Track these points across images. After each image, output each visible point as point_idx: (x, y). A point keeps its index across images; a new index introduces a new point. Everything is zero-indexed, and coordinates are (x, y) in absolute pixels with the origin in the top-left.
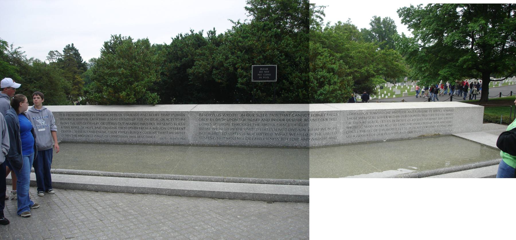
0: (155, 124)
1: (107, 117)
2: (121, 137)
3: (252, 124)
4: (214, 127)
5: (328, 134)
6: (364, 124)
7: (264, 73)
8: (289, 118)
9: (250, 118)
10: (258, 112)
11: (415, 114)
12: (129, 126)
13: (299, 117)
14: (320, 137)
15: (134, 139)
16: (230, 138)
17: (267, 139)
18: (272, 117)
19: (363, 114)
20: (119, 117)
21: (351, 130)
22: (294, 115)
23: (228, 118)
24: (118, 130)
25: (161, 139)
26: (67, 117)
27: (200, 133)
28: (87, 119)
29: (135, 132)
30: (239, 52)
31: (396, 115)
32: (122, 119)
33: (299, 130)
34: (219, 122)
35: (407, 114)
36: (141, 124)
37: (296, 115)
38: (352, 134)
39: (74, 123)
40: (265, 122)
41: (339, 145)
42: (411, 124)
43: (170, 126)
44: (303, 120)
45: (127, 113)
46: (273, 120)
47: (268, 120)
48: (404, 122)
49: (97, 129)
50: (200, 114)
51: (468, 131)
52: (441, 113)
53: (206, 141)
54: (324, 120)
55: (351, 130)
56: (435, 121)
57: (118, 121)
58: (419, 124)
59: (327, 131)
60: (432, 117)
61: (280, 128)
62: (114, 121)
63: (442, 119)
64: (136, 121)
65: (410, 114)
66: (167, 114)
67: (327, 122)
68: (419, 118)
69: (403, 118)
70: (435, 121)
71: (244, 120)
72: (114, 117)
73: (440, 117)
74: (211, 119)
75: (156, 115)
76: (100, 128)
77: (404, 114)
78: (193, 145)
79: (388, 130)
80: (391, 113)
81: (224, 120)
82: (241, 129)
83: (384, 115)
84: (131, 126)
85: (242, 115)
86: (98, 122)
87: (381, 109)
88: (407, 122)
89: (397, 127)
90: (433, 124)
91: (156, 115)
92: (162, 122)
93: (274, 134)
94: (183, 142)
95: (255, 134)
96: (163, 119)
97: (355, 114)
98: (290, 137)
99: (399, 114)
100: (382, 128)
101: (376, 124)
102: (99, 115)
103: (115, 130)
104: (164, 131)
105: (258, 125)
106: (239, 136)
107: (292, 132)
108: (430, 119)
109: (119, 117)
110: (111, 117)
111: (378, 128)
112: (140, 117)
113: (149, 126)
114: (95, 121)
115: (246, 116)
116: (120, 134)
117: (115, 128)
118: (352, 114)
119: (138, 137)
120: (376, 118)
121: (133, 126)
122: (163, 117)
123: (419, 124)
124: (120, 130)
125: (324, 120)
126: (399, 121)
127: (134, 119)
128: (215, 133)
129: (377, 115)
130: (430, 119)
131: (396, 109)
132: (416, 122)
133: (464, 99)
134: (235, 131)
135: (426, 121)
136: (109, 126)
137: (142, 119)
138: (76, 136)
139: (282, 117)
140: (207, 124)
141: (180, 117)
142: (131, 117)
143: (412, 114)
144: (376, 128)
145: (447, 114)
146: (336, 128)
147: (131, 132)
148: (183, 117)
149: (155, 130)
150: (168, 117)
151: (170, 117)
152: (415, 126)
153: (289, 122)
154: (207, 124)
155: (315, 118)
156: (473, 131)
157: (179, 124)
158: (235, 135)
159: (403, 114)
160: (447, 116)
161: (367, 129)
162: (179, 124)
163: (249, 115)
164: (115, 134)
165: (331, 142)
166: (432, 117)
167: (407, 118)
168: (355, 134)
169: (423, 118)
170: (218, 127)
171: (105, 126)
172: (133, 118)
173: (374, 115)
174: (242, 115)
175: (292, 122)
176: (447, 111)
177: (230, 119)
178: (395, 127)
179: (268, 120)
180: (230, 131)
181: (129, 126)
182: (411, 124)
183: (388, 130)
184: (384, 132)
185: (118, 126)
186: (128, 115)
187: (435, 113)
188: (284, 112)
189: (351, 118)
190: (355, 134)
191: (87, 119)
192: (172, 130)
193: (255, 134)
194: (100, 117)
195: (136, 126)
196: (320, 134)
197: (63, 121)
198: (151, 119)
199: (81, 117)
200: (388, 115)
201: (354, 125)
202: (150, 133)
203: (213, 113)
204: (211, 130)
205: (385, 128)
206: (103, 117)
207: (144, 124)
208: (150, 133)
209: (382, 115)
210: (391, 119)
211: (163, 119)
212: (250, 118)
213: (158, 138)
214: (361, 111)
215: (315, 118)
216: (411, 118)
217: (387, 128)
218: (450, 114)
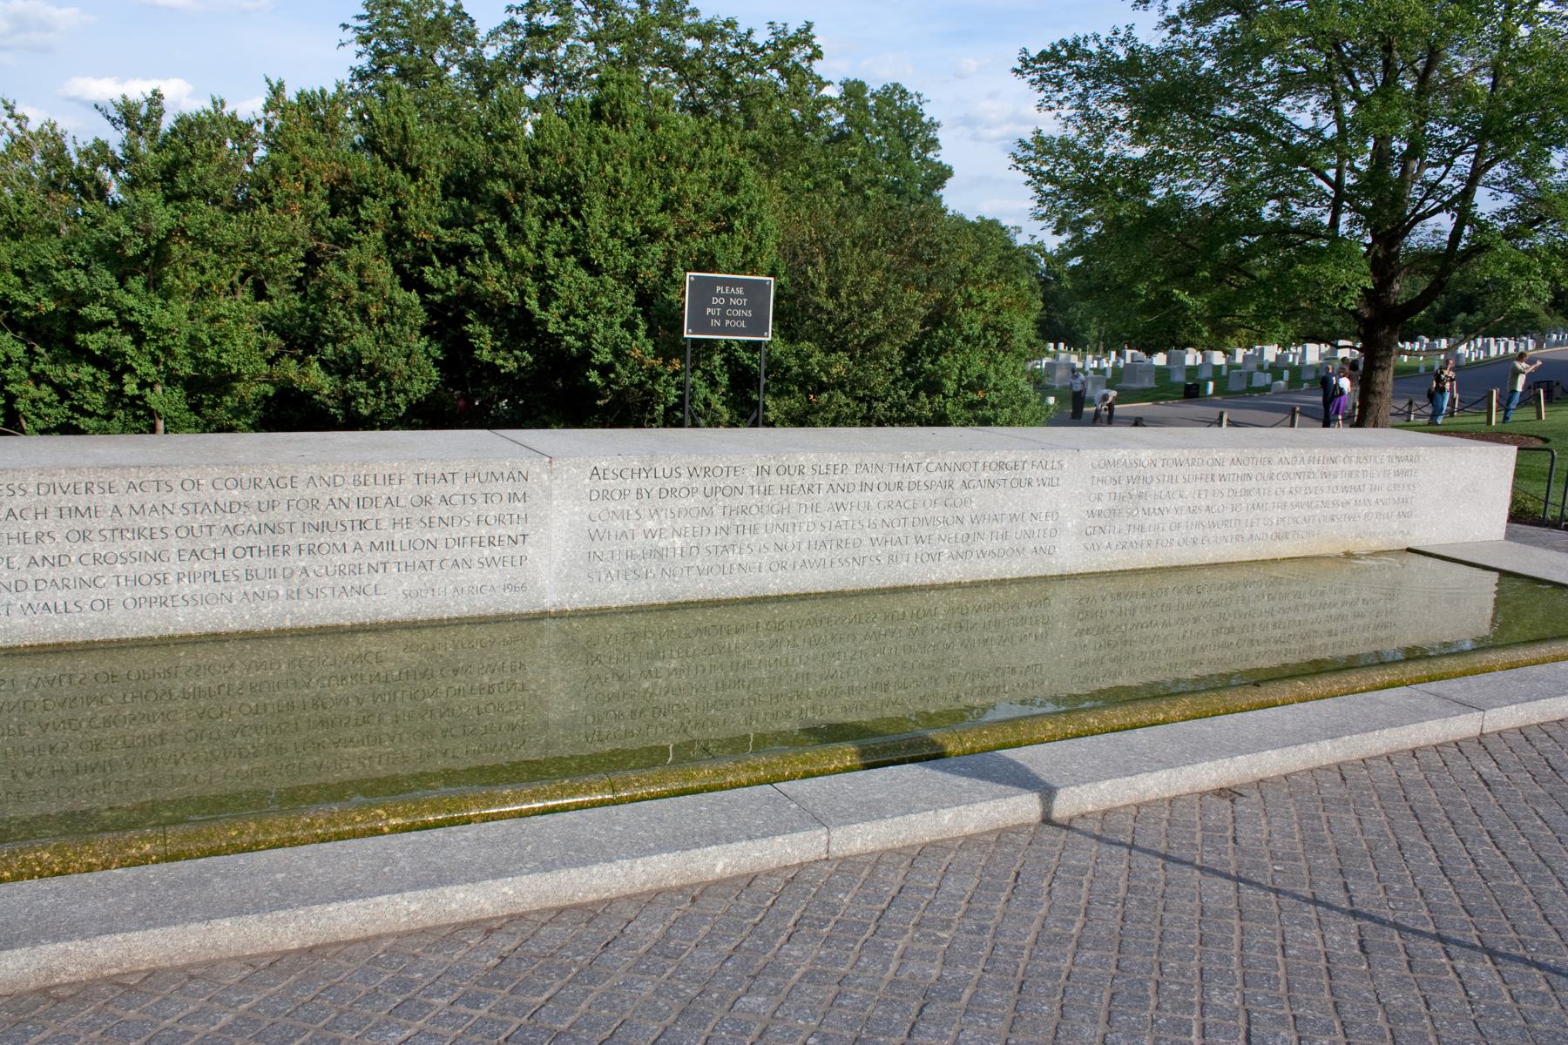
0: (385, 524)
1: (110, 500)
4: (650, 524)
5: (1029, 535)
6: (1143, 504)
7: (727, 305)
8: (915, 478)
12: (241, 541)
13: (945, 475)
14: (1006, 545)
16: (710, 570)
20: (181, 498)
21: (1102, 522)
22: (932, 467)
23: (709, 483)
24: (173, 567)
27: (592, 556)
30: (46, 856)
34: (671, 503)
36: (306, 526)
38: (1104, 539)
43: (457, 532)
44: (957, 485)
46: (864, 486)
49: (42, 571)
55: (1102, 522)
57: (179, 518)
58: (1309, 505)
59: (1029, 525)
61: (888, 515)
62: (155, 521)
64: (280, 515)
67: (1027, 492)
68: (1311, 483)
76: (58, 562)
80: (1227, 464)
82: (754, 530)
84: (252, 539)
86: (47, 525)
92: (418, 513)
95: (804, 546)
101: (1180, 502)
103: (155, 567)
104: (425, 555)
105: (815, 508)
106: (746, 558)
107: (924, 531)
109: (181, 498)
113: (350, 538)
114: (30, 527)
115: (773, 476)
116: (187, 588)
117: (158, 557)
119: (289, 597)
120: (1181, 480)
121: (262, 541)
122: (424, 490)
124: (186, 567)
127: (272, 505)
128: (658, 554)
130: (1345, 489)
133: (1433, 422)
134: (730, 538)
136: (118, 547)
137: (314, 504)
142: (254, 496)
145: (1397, 473)
146: (1054, 514)
147: (250, 575)
149: (379, 556)
150: (448, 490)
153: (916, 493)
155: (993, 476)
160: (1398, 480)
161: (1149, 521)
164: (156, 591)
166: (1352, 482)
167: (1275, 485)
169: (1324, 483)
171: (98, 547)
172: (262, 496)
177: (714, 491)
180: (712, 540)
181: (241, 541)
183: (1213, 525)
184: (1199, 533)
185: (174, 544)
193: (804, 546)
195: (280, 539)
201: (1112, 504)
202: (356, 570)
204: (640, 538)
206: (82, 501)
207: (321, 528)
208: (356, 570)
210: (1227, 485)
211: (425, 501)
212: (786, 480)
215: (993, 476)
218: (1405, 473)
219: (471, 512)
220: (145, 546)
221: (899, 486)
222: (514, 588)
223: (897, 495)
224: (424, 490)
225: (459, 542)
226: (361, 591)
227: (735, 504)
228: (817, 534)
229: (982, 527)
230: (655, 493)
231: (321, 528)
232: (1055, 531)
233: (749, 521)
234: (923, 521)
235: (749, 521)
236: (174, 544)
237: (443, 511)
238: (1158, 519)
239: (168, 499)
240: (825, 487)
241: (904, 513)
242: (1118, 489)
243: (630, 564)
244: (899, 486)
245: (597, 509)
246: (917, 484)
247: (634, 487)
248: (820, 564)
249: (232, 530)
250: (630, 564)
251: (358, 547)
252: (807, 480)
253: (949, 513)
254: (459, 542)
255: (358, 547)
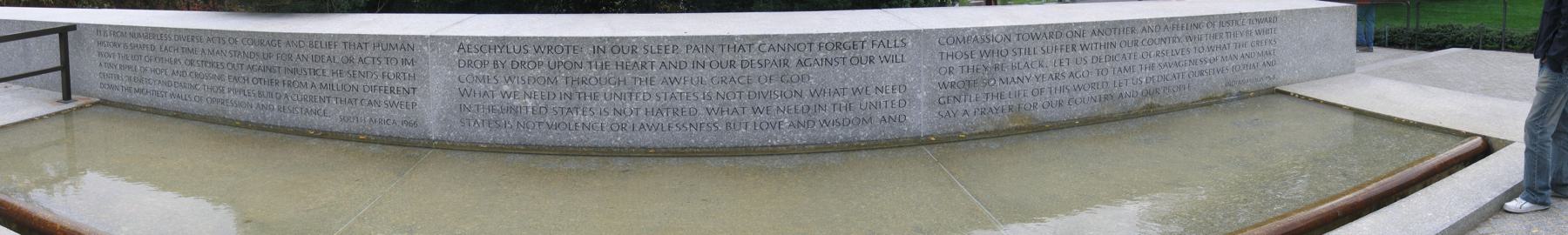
1: (201, 46)
2: (234, 103)
3: (629, 80)
4: (506, 88)
5: (877, 105)
6: (999, 74)
8: (747, 57)
9: (622, 58)
10: (648, 38)
11: (1164, 34)
12: (255, 75)
13: (780, 55)
14: (851, 115)
15: (269, 115)
17: (681, 127)
18: (692, 56)
19: (994, 39)
20: (229, 48)
21: (956, 92)
23: (552, 58)
24: (228, 85)
25: (343, 119)
26: (110, 39)
27: (462, 108)
28: (153, 48)
29: (270, 95)
31: (1103, 39)
32: (236, 53)
33: (783, 94)
34: (521, 71)
35: (1140, 36)
37: (771, 48)
38: (960, 107)
39: (126, 57)
40: (673, 73)
41: (918, 142)
42: (1152, 67)
45: (251, 37)
46: (696, 64)
47: (679, 66)
48: (1132, 62)
49: (177, 78)
50: (462, 44)
51: (1318, 75)
52: (1242, 29)
53: (484, 134)
54: (860, 61)
55: (956, 92)
56: (1227, 53)
57: (228, 59)
58: (1177, 64)
59: (874, 98)
60: (1217, 42)
61: (722, 89)
62: (218, 59)
63: (1244, 45)
64: (273, 62)
65: (1149, 35)
66: (361, 42)
68: (1177, 46)
69: (1126, 50)
70: (1227, 53)
71: (605, 66)
72: (216, 46)
73: (1240, 39)
74: (495, 63)
75: (329, 45)
76: (183, 74)
77: (1130, 38)
78: (444, 146)
79: (1078, 88)
80: (1088, 35)
81: (538, 65)
82: (594, 97)
83: (1064, 40)
84: (260, 75)
85: (597, 50)
87: (1062, 21)
88: (1140, 61)
89: (1110, 78)
90: (1219, 64)
91: (329, 45)
92: (346, 68)
93: (702, 111)
94: (412, 133)
95: (641, 112)
96: (350, 60)
97: (965, 40)
98: (752, 118)
99: (1113, 38)
100: (1060, 84)
101: (1040, 71)
102: (180, 38)
103: (219, 83)
104: (352, 95)
105: (650, 81)
106: (588, 119)
107: (761, 103)
108: (1211, 49)
109: (229, 48)
110: (209, 46)
111: (1046, 84)
112: (285, 49)
113: (309, 79)
114: (173, 55)
116: (233, 96)
117: (220, 78)
118: (956, 41)
122: (349, 53)
123: (1177, 64)
125: (860, 61)
126: (1113, 58)
127: (270, 56)
129: (1040, 43)
130: (1211, 49)
131: (1102, 23)
132: (1167, 59)
135: (1198, 56)
136: (204, 70)
137: (290, 57)
138: (129, 89)
139: (728, 56)
140: (483, 79)
141: (400, 55)
142: (261, 50)
143: (1154, 36)
144: (1039, 85)
145: (1258, 33)
146: (903, 87)
147: (260, 94)
148: (409, 55)
149: (325, 93)
151: (369, 52)
152: (1165, 71)
153: (750, 71)
154: (483, 79)
156: (1333, 75)
157: (397, 76)
158: (575, 117)
159: (1125, 38)
160: (1259, 38)
162: (397, 76)
163: (621, 50)
164: (220, 96)
165: (889, 132)
166: (1217, 42)
167: (1140, 50)
168: (970, 106)
169: (1190, 45)
170: (520, 88)
173: (1031, 44)
174: (597, 50)
175: (758, 71)
176: (1259, 21)
178: (1101, 78)
179: (679, 66)
180: (559, 103)
181: (255, 75)
182: (1152, 67)
183: (1078, 88)
184: (1065, 96)
185: (227, 73)
186: (254, 42)
187: (1224, 30)
188: (731, 38)
189: (954, 56)
190: (970, 106)
191: (153, 48)
192: (376, 95)
193: (641, 112)
194: (183, 44)
195: (275, 76)
196: (849, 107)
197: (103, 50)
198: (315, 59)
199: (142, 41)
200: (1078, 40)
201: (967, 76)
202: (312, 99)
203: (502, 43)
204: (498, 97)
205: (1069, 82)
206: (190, 45)
207: (294, 71)
208: (312, 99)
209: (1058, 42)
210: (1089, 54)
211: (350, 60)
212: (622, 58)
213: (333, 116)
214: (988, 29)
216: (1154, 49)
217: (1076, 82)
218: (1267, 32)
219: (379, 69)
220: (215, 72)
221: (732, 64)
222: (408, 124)
223: (730, 72)
224: (349, 53)
225: (373, 89)
226: (316, 112)
227: (576, 75)
228: (653, 102)
229: (822, 100)
230: (508, 64)
231: (294, 71)
232: (903, 103)
233: (589, 89)
234: (758, 95)
235: (589, 89)
236: (227, 73)
237: (361, 67)
238: (1018, 87)
239: (224, 47)
240: (658, 64)
241: (739, 87)
242: (970, 62)
243: (492, 116)
244: (732, 64)
245: (465, 73)
246: (751, 63)
247: (491, 60)
248: (657, 127)
249: (251, 68)
250: (492, 116)
251: (313, 85)
252: (640, 59)
253: (786, 87)
254: (373, 89)
255: (313, 85)
